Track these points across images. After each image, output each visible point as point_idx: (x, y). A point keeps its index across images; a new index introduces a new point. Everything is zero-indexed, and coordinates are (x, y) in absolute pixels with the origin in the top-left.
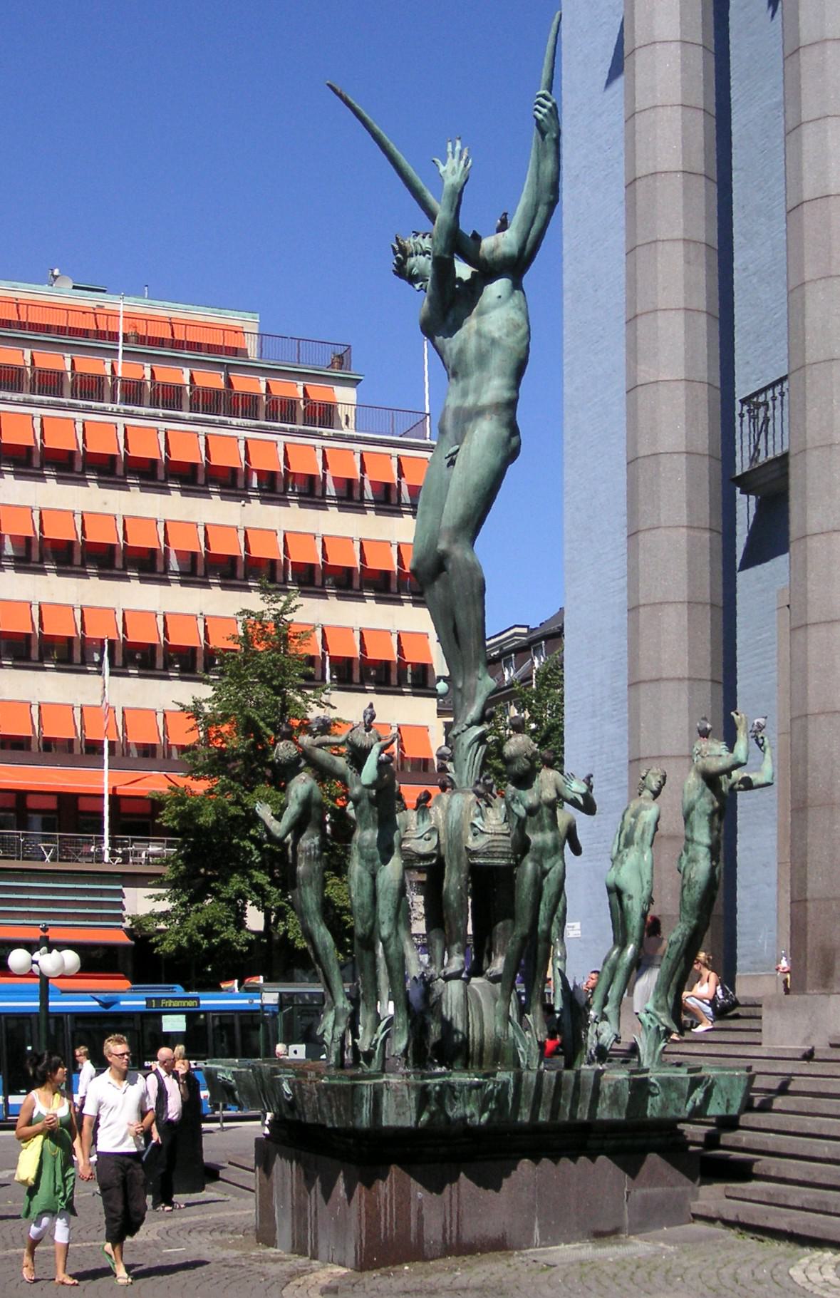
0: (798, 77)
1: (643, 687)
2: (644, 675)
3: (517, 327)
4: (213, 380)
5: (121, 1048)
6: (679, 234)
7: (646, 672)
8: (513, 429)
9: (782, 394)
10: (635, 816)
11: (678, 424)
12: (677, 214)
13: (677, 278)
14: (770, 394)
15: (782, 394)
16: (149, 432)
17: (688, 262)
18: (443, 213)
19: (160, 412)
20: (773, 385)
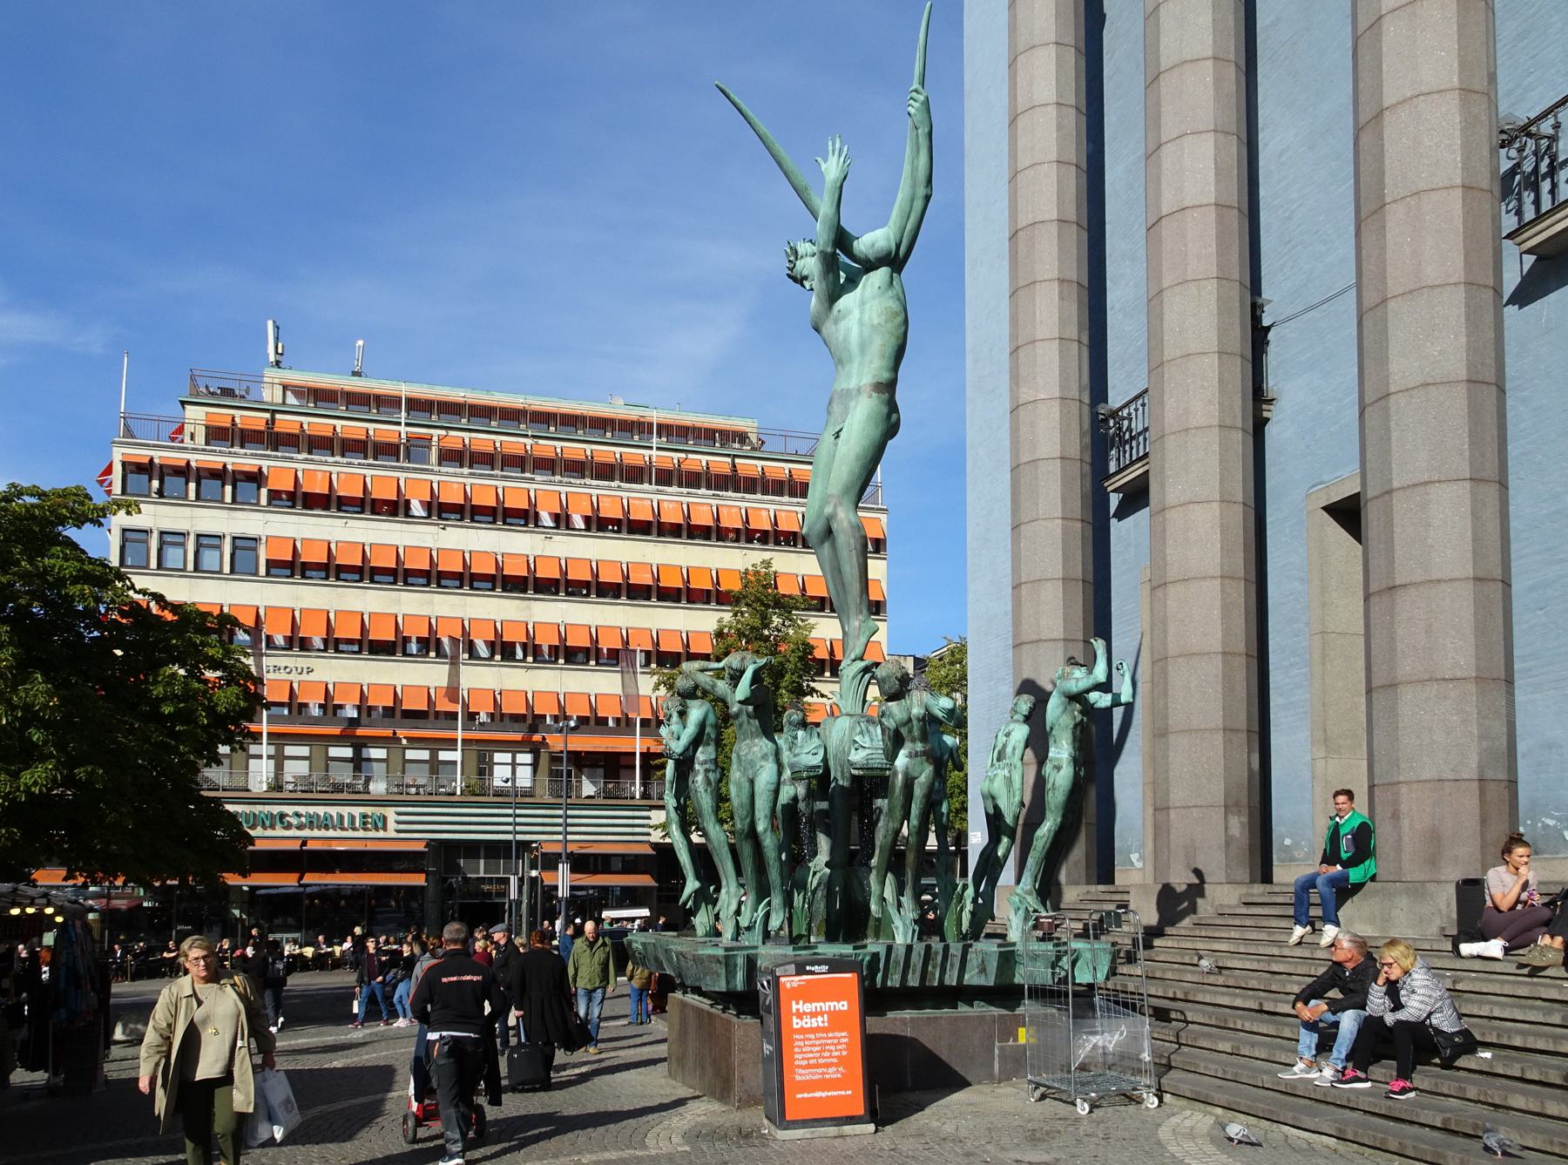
0: (1158, 104)
1: (1025, 648)
2: (1025, 638)
3: (897, 314)
4: (721, 464)
5: (196, 953)
6: (1055, 274)
7: (1028, 634)
8: (892, 407)
9: (1143, 405)
10: (1008, 735)
11: (1054, 435)
12: (1054, 258)
13: (1053, 313)
14: (1133, 407)
15: (1143, 405)
16: (672, 502)
17: (1061, 298)
18: (825, 207)
19: (685, 490)
20: (1136, 398)
